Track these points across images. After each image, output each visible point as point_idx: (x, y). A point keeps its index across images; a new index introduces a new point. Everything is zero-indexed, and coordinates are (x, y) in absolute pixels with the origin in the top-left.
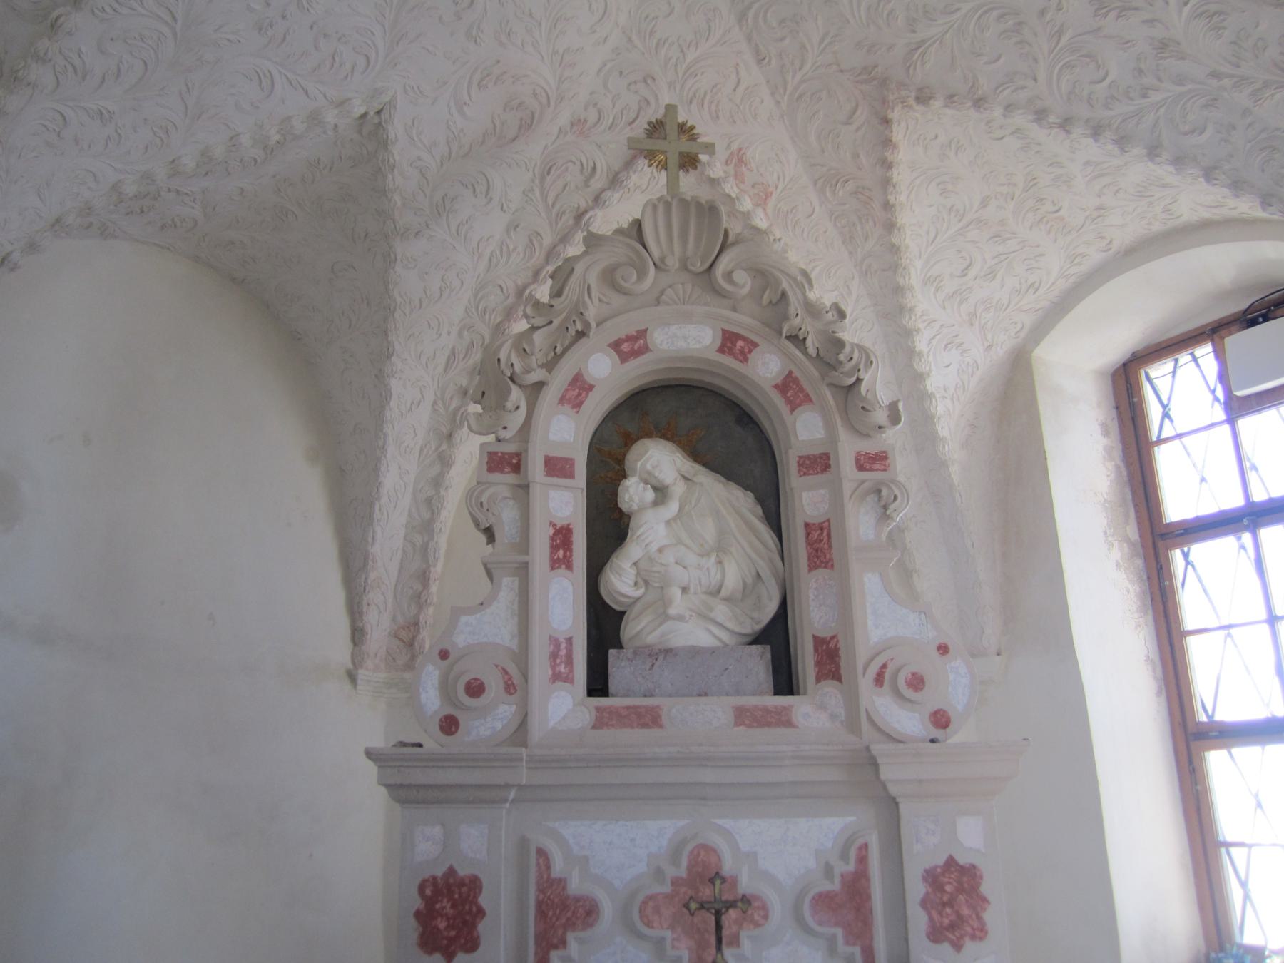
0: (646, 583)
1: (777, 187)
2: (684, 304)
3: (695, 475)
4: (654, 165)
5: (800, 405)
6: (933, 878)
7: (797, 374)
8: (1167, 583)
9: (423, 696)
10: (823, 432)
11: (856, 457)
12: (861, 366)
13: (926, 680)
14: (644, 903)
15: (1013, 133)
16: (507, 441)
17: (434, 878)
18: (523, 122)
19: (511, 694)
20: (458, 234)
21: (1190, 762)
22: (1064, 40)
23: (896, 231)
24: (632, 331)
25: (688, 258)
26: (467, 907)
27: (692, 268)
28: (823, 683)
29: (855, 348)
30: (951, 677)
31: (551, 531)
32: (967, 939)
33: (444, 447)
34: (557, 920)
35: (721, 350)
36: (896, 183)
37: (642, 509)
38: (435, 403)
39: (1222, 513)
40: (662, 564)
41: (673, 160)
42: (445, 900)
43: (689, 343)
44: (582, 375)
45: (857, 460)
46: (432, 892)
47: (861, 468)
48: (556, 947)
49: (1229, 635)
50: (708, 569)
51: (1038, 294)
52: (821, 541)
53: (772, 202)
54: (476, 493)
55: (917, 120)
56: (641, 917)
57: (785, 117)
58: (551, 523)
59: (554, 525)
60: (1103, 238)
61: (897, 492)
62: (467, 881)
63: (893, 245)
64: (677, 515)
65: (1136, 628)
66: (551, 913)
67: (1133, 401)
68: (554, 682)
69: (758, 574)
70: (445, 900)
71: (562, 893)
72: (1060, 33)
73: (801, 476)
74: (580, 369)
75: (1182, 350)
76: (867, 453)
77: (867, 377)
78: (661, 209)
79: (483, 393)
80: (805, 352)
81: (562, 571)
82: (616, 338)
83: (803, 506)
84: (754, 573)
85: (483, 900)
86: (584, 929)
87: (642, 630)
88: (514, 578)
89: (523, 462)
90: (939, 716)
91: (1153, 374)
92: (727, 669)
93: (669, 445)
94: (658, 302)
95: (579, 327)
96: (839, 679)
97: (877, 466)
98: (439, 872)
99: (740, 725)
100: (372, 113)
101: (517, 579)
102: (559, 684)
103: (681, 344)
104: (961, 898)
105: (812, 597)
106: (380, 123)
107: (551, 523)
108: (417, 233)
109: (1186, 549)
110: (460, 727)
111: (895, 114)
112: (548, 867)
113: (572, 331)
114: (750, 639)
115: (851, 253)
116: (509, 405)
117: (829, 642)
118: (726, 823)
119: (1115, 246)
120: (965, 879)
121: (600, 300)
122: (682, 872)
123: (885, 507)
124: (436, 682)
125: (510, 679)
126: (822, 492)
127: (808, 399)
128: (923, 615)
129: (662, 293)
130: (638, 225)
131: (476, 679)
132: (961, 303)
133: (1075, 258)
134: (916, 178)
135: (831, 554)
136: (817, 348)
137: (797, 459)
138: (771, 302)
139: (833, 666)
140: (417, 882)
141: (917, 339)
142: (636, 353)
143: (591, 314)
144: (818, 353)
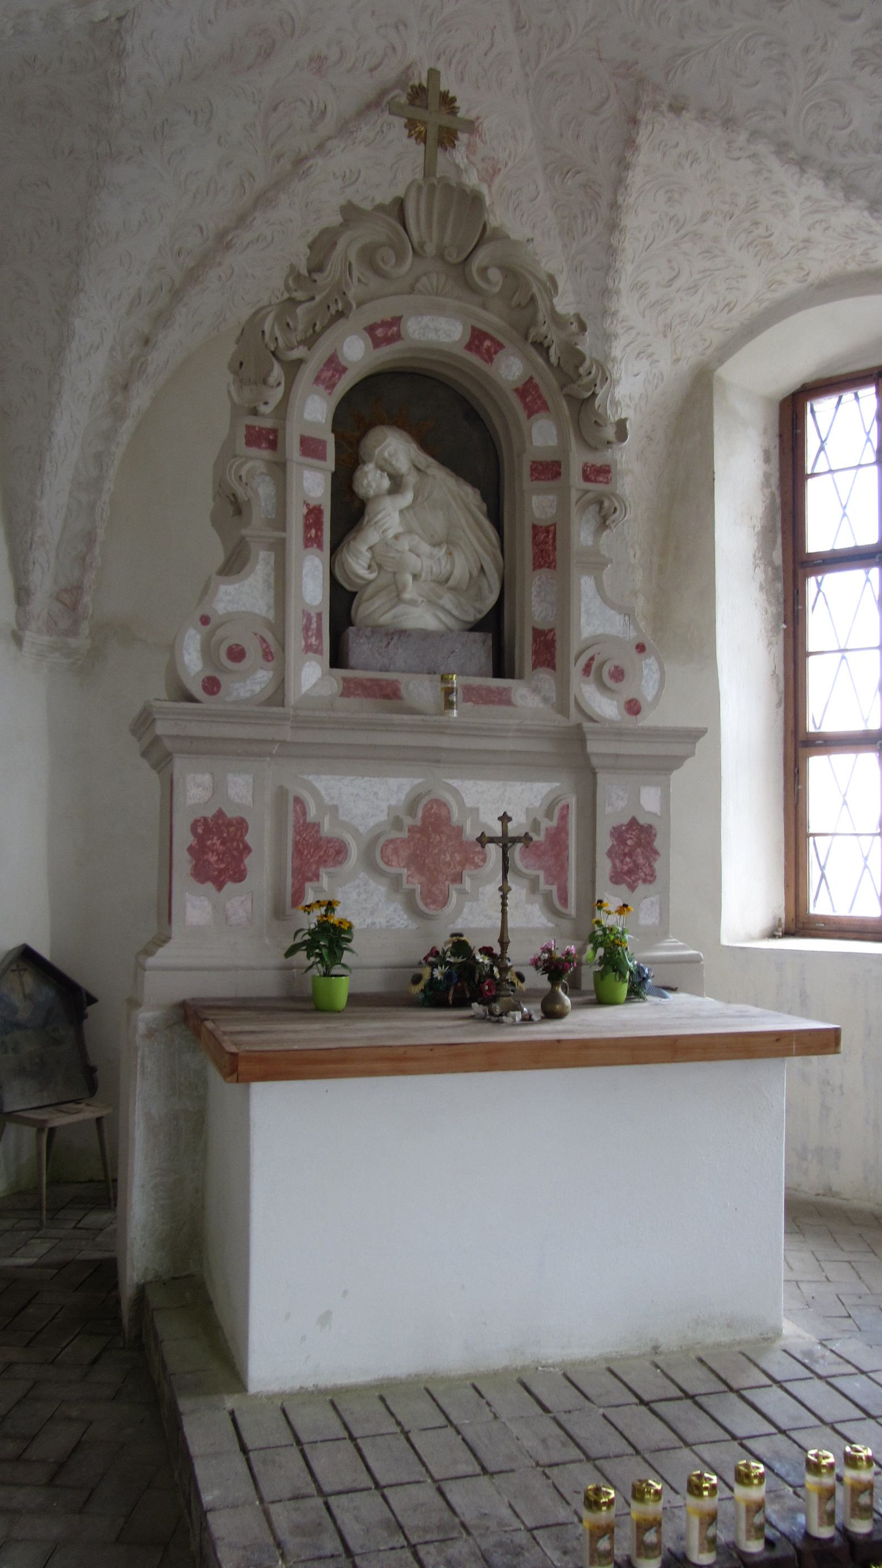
0: (380, 567)
1: (506, 164)
2: (436, 295)
3: (428, 467)
4: (414, 136)
5: (537, 412)
6: (618, 834)
7: (537, 380)
8: (800, 607)
9: (187, 658)
10: (556, 440)
11: (583, 469)
12: (598, 382)
13: (625, 673)
14: (385, 845)
15: (749, 157)
16: (263, 415)
17: (205, 819)
18: (263, 51)
19: (268, 661)
20: (169, 163)
21: (796, 765)
22: (821, 80)
23: (617, 233)
24: (388, 317)
25: (446, 247)
26: (235, 844)
27: (449, 259)
28: (540, 669)
29: (594, 363)
30: (645, 672)
31: (305, 511)
32: (640, 882)
33: (119, 399)
34: (311, 857)
35: (469, 347)
36: (628, 185)
37: (378, 496)
38: (113, 349)
39: (856, 548)
40: (397, 551)
41: (432, 135)
42: (215, 838)
43: (439, 337)
44: (337, 358)
45: (584, 471)
46: (203, 830)
47: (586, 478)
48: (310, 880)
49: (843, 658)
50: (439, 559)
51: (730, 314)
52: (546, 543)
53: (498, 180)
54: (234, 467)
55: (664, 125)
56: (382, 858)
57: (530, 92)
58: (305, 502)
59: (308, 505)
60: (802, 269)
61: (617, 504)
62: (234, 822)
63: (610, 246)
64: (411, 505)
65: (768, 646)
66: (306, 852)
67: (796, 433)
68: (306, 652)
69: (482, 567)
70: (215, 838)
71: (315, 835)
72: (819, 72)
73: (532, 481)
74: (336, 350)
75: (849, 388)
76: (593, 466)
77: (601, 392)
78: (424, 191)
79: (241, 364)
80: (547, 359)
81: (314, 549)
82: (371, 322)
83: (532, 508)
84: (479, 566)
85: (249, 839)
86: (334, 866)
87: (375, 611)
88: (270, 553)
89: (279, 440)
90: (632, 704)
91: (816, 408)
92: (453, 652)
93: (404, 434)
94: (412, 290)
95: (340, 307)
96: (554, 668)
97: (601, 479)
98: (210, 813)
99: (468, 701)
100: (113, 19)
101: (273, 554)
102: (310, 654)
103: (432, 336)
104: (639, 850)
105: (534, 593)
106: (118, 31)
107: (305, 502)
108: (129, 159)
109: (819, 578)
110: (221, 689)
111: (644, 117)
112: (304, 814)
113: (333, 310)
114: (469, 626)
115: (565, 246)
116: (272, 380)
117: (547, 635)
118: (455, 783)
119: (811, 278)
120: (643, 836)
121: (359, 280)
122: (418, 822)
123: (605, 519)
124: (198, 647)
125: (268, 647)
126: (551, 497)
127: (545, 407)
128: (627, 618)
129: (417, 280)
130: (399, 206)
131: (238, 645)
132: (660, 314)
133: (772, 285)
134: (648, 182)
135: (554, 556)
136: (559, 358)
137: (530, 464)
138: (519, 305)
139: (548, 655)
140: (191, 821)
141: (615, 344)
142: (389, 340)
143: (353, 293)
144: (559, 363)
